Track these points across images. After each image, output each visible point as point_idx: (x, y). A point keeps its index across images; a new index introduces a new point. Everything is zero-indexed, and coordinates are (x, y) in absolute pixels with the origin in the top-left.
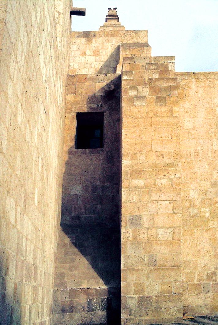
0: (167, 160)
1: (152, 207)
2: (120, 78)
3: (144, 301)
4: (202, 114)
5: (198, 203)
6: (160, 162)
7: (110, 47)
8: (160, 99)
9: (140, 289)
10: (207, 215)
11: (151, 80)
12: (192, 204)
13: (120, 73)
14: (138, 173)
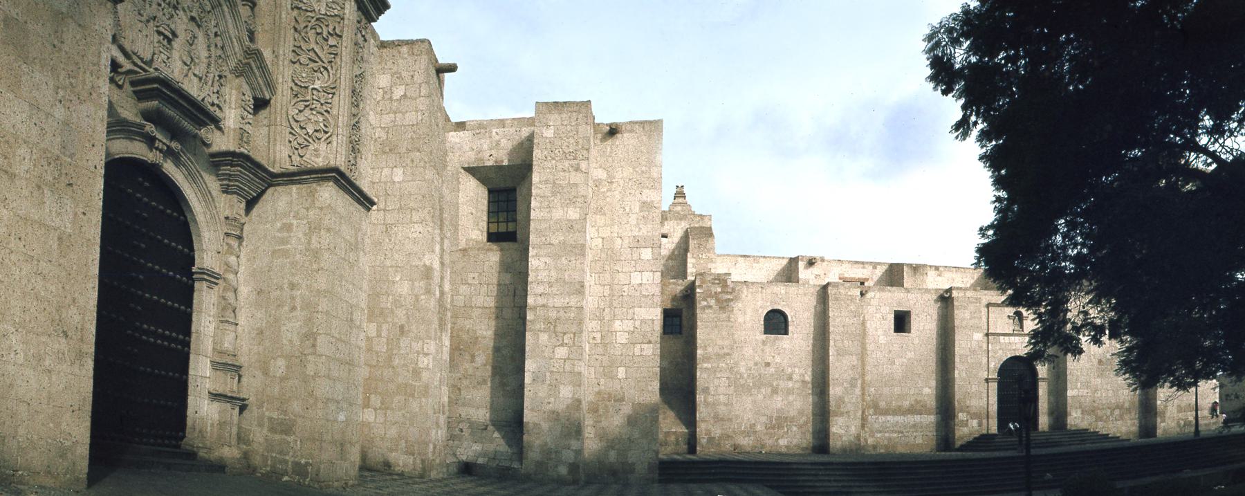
0: (726, 350)
1: (716, 382)
2: (692, 286)
3: (711, 440)
4: (749, 311)
5: (745, 376)
6: (721, 352)
7: (680, 230)
8: (722, 308)
9: (708, 432)
10: (751, 384)
11: (716, 293)
12: (741, 376)
13: (693, 278)
14: (707, 359)
